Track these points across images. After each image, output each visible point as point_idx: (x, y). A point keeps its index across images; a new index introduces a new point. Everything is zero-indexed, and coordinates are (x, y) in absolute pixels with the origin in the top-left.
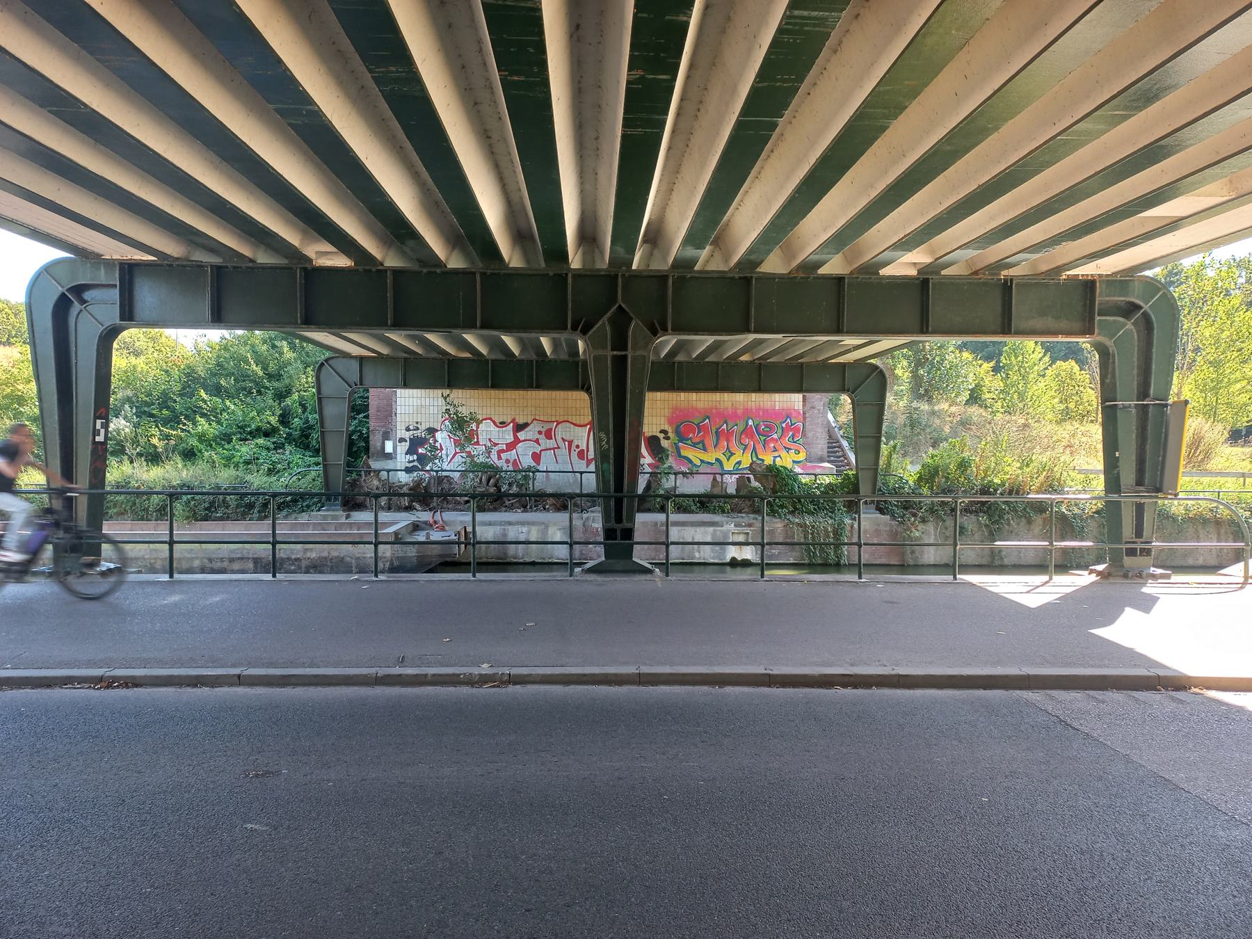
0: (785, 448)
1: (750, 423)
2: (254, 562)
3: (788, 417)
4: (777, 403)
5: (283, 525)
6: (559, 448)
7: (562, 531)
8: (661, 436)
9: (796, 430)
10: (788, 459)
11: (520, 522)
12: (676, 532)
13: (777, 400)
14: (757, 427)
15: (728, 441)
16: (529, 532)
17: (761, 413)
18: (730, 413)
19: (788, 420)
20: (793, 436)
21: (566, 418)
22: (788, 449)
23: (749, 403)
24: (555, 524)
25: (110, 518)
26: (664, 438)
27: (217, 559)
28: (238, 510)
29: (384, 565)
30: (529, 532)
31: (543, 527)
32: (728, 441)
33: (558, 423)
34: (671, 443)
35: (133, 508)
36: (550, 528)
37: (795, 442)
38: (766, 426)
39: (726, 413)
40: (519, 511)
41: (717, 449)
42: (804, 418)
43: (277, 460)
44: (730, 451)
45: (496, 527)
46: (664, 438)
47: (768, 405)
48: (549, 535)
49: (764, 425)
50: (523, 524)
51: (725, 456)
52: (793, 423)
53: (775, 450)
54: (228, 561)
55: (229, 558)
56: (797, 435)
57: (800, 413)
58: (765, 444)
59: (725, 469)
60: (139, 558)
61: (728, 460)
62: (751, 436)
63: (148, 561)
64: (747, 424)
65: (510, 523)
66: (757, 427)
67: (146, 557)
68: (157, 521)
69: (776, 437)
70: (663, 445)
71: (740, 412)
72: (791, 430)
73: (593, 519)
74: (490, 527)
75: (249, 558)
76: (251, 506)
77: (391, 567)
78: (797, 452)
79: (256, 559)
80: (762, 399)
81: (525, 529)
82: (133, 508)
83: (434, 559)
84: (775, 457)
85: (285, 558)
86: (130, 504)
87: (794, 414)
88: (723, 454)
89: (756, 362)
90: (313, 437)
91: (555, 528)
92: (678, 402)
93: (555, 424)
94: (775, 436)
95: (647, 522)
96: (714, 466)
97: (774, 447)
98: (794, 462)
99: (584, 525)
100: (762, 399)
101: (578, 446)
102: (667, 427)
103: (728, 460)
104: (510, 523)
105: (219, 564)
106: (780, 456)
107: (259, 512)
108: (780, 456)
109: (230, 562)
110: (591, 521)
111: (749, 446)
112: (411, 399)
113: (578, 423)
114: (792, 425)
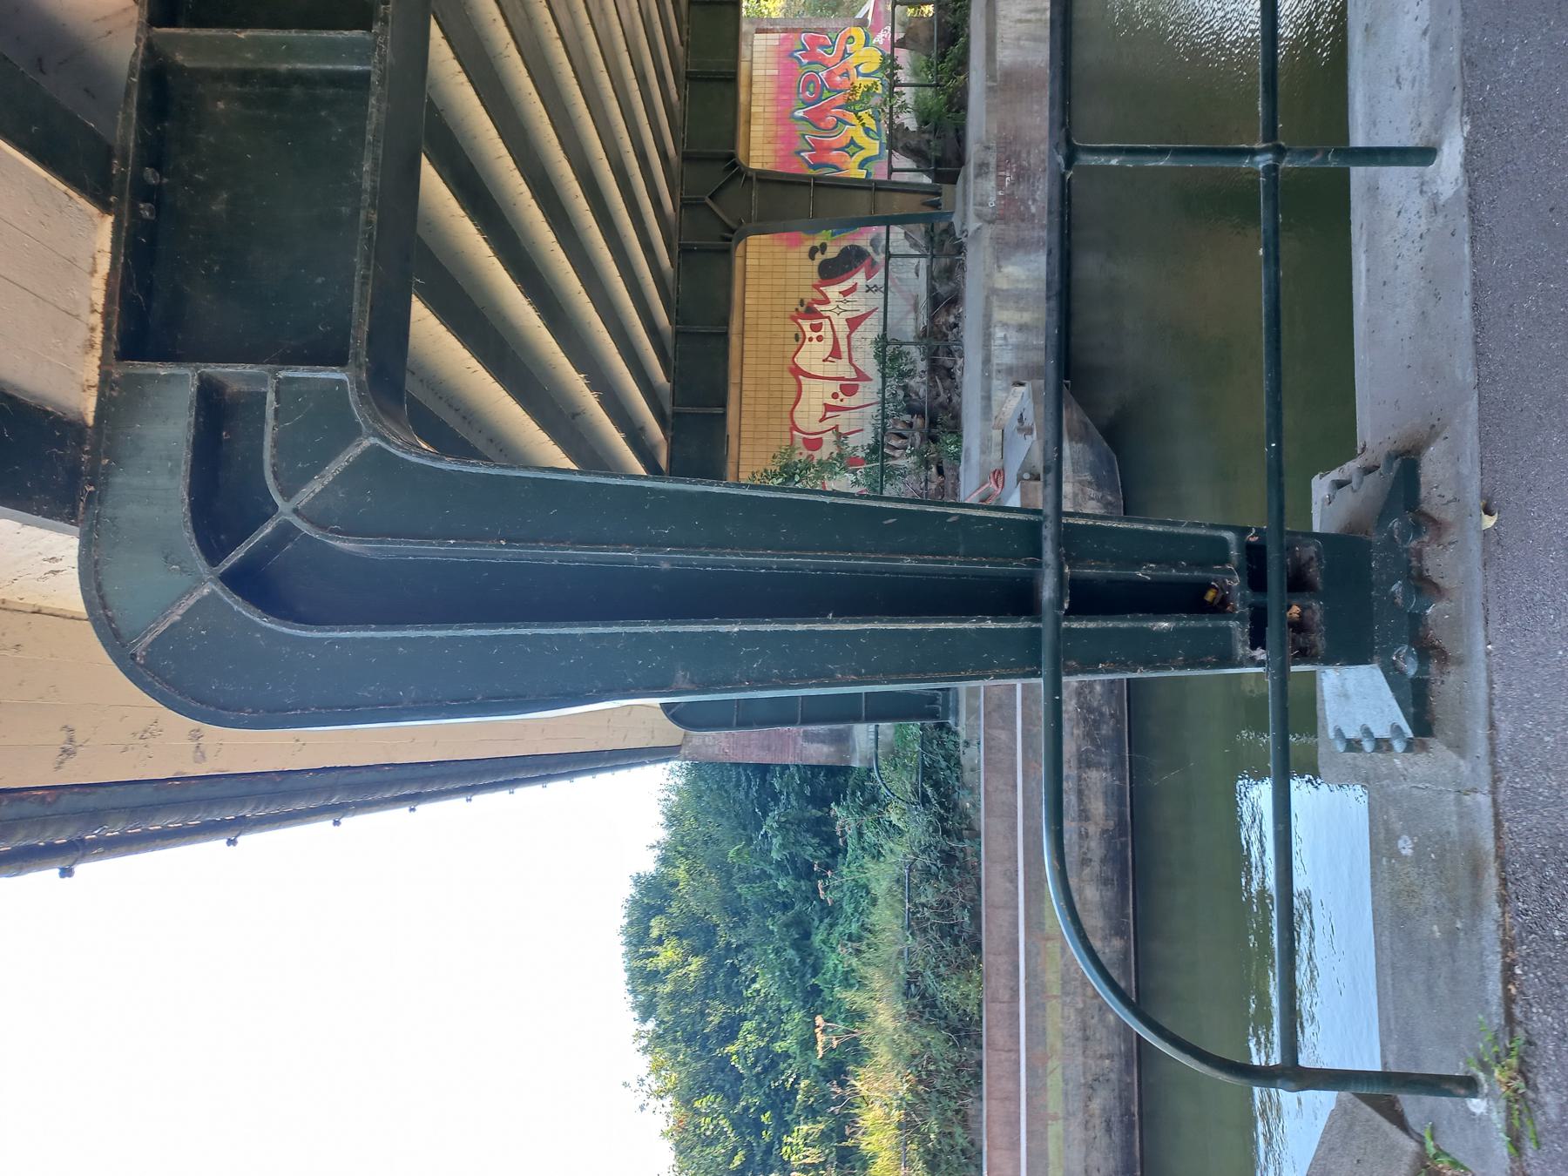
0: (843, 58)
1: (801, 114)
2: (1089, 767)
3: (791, 55)
4: (770, 72)
5: (990, 789)
6: (836, 427)
7: (1002, 263)
8: (819, 257)
9: (813, 42)
10: (861, 53)
11: (984, 341)
12: (1007, 52)
13: (762, 72)
14: (807, 103)
15: (830, 149)
16: (1005, 325)
17: (785, 97)
18: (783, 146)
19: (797, 54)
20: (823, 46)
21: (786, 415)
22: (845, 54)
23: (767, 115)
24: (989, 276)
25: (973, 1145)
26: (823, 254)
27: (1081, 847)
28: (958, 879)
29: (1093, 499)
30: (1005, 325)
31: (994, 299)
32: (830, 149)
33: (794, 427)
34: (831, 241)
35: (954, 1094)
36: (997, 286)
37: (834, 44)
38: (806, 88)
39: (782, 153)
40: (960, 362)
41: (844, 167)
42: (794, 30)
43: (853, 906)
44: (847, 146)
45: (993, 388)
46: (823, 254)
47: (770, 88)
48: (1010, 287)
49: (804, 91)
50: (988, 337)
51: (854, 154)
52: (801, 47)
53: (846, 73)
54: (1084, 824)
55: (1080, 820)
56: (821, 40)
57: (785, 39)
58: (835, 89)
59: (877, 152)
60: (1084, 1022)
61: (862, 149)
62: (823, 112)
63: (1088, 1001)
64: (802, 119)
65: (987, 361)
66: (807, 103)
67: (1080, 1005)
68: (980, 1047)
69: (825, 73)
70: (835, 255)
71: (781, 130)
72: (813, 50)
73: (981, 204)
74: (993, 398)
75: (1080, 778)
76: (948, 858)
77: (1095, 487)
78: (851, 40)
79: (1080, 761)
80: (761, 97)
81: (999, 333)
82: (954, 1094)
83: (1075, 416)
84: (859, 74)
85: (1078, 700)
86: (945, 1101)
87: (787, 46)
88: (852, 156)
89: (685, 39)
90: (811, 855)
91: (997, 275)
92: (767, 97)
93: (795, 433)
94: (823, 74)
95: (988, 105)
96: (871, 171)
97: (841, 75)
98: (866, 45)
99: (991, 222)
100: (761, 97)
101: (835, 396)
102: (806, 248)
103: (862, 149)
104: (987, 361)
105: (1093, 844)
106: (857, 67)
107: (960, 839)
108: (857, 67)
109: (1087, 819)
110: (985, 210)
111: (841, 116)
112: (760, 328)
113: (794, 395)
114: (805, 49)
